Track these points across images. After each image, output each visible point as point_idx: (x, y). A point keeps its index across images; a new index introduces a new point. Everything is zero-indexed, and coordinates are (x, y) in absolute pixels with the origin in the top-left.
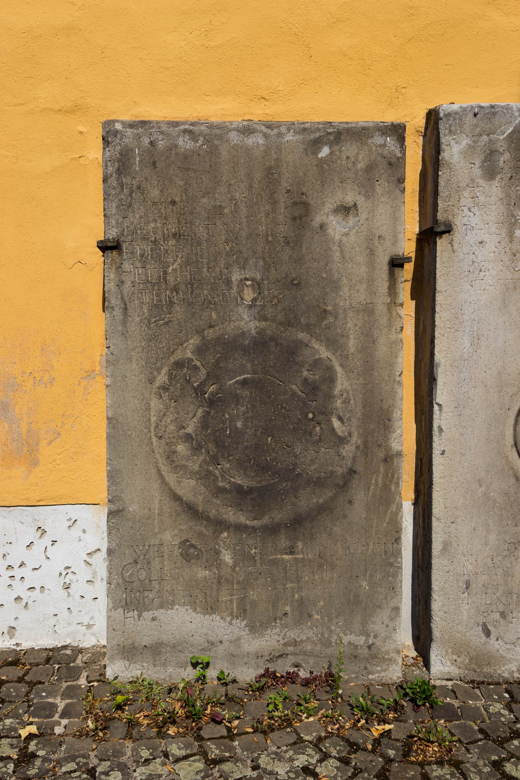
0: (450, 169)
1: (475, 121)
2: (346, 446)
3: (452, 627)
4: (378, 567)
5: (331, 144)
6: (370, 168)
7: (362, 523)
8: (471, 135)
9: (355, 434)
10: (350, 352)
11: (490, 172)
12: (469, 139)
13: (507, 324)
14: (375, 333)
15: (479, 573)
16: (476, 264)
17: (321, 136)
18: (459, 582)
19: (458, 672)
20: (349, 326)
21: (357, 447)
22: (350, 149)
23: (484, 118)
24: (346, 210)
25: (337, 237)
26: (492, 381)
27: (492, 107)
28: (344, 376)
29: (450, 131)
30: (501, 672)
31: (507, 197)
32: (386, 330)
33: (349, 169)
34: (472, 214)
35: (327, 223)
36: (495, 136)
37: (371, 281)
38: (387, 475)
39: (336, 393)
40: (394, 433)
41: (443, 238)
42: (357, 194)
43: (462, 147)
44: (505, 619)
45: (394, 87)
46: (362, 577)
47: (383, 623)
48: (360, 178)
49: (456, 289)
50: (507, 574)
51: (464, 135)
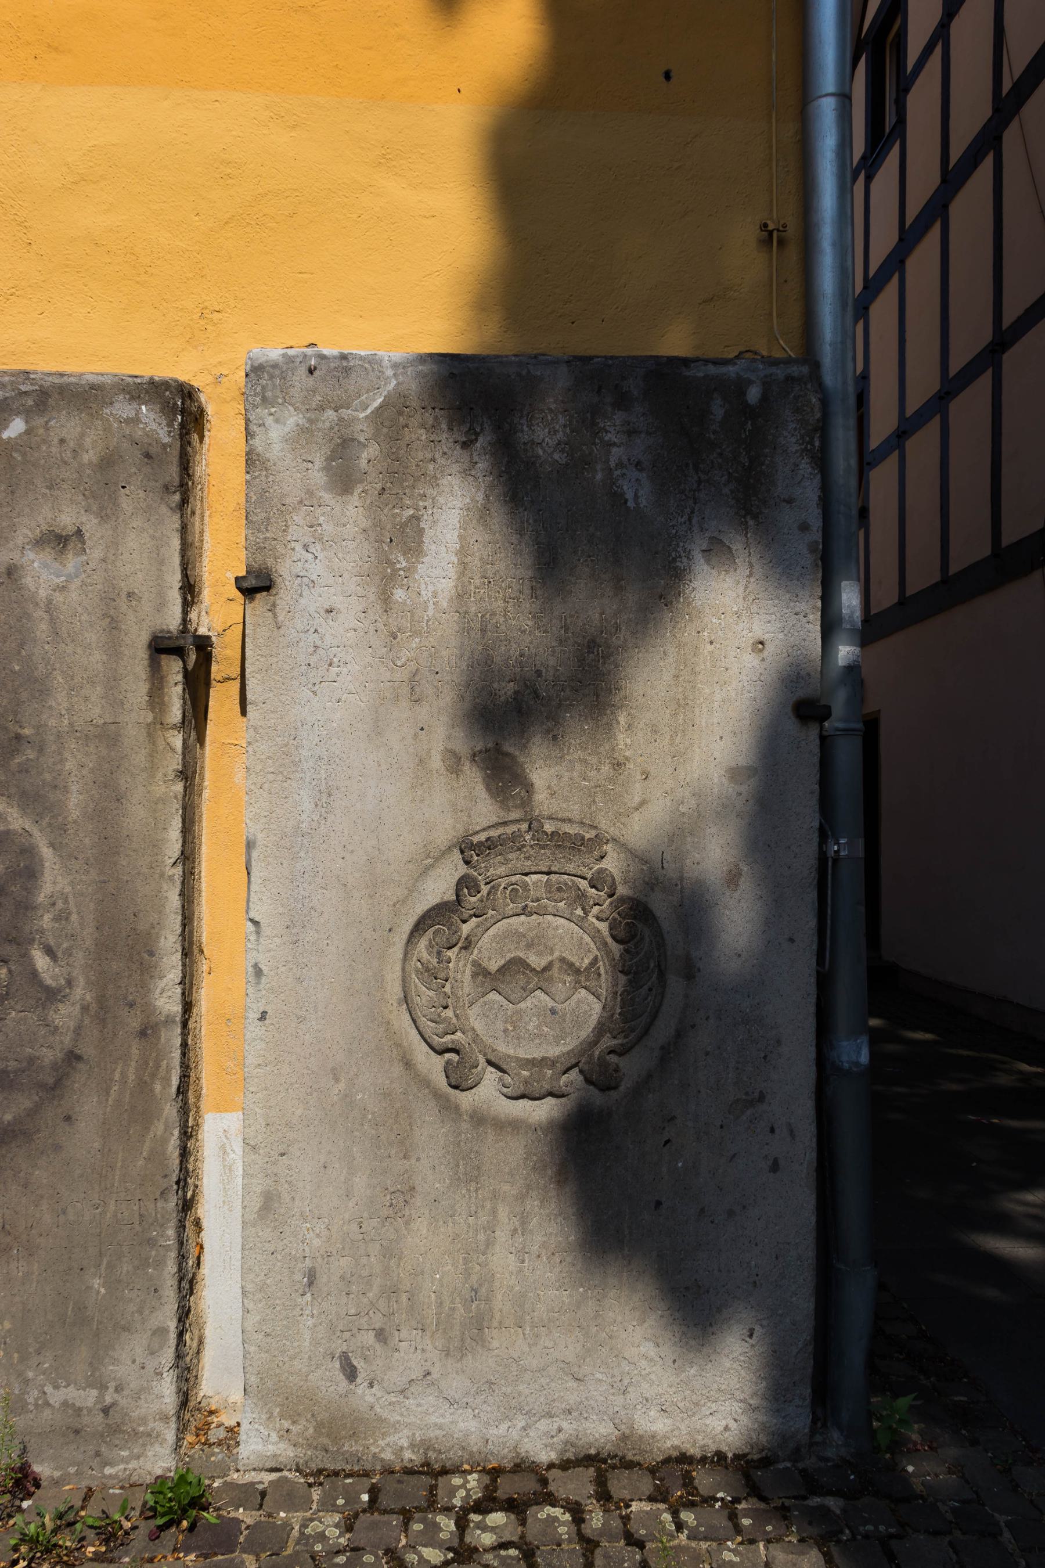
0: (267, 469)
1: (311, 381)
2: (60, 1006)
3: (281, 1364)
4: (126, 1249)
5: (27, 414)
6: (108, 462)
7: (92, 1160)
8: (303, 408)
9: (82, 980)
10: (70, 819)
11: (343, 481)
12: (301, 416)
13: (384, 767)
14: (122, 782)
15: (335, 1253)
16: (321, 651)
17: (6, 398)
18: (293, 1273)
19: (292, 1455)
20: (67, 768)
21: (85, 1009)
22: (67, 425)
23: (328, 378)
24: (60, 541)
25: (43, 593)
26: (357, 875)
27: (344, 357)
28: (57, 867)
29: (264, 399)
30: (377, 1450)
31: (376, 526)
32: (144, 775)
33: (65, 463)
34: (310, 557)
35: (22, 566)
36: (349, 412)
37: (112, 682)
38: (147, 1063)
39: (40, 900)
40: (161, 978)
41: (257, 601)
42: (82, 512)
43: (287, 430)
44: (385, 1343)
45: (197, 310)
46: (93, 1270)
47: (134, 1362)
48: (87, 480)
49: (283, 698)
50: (389, 1253)
51: (290, 408)
